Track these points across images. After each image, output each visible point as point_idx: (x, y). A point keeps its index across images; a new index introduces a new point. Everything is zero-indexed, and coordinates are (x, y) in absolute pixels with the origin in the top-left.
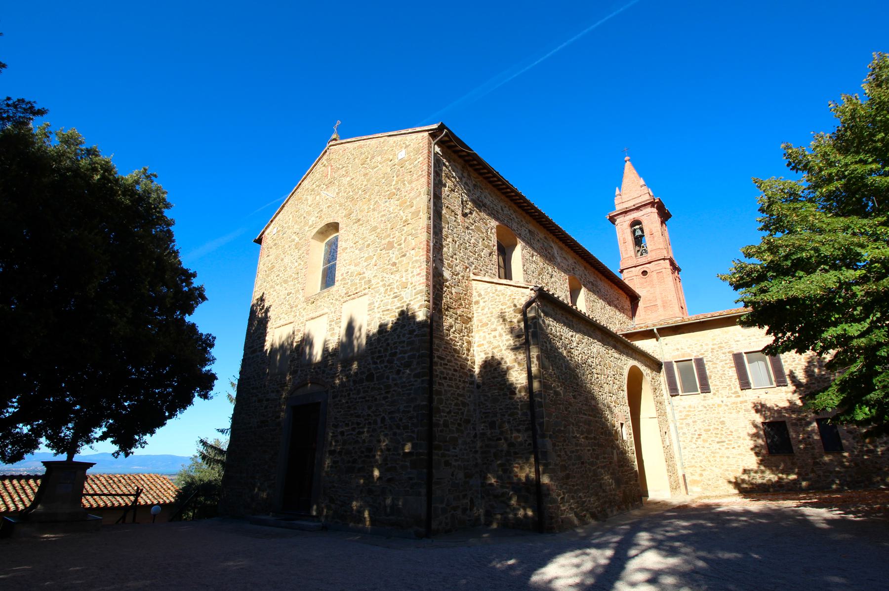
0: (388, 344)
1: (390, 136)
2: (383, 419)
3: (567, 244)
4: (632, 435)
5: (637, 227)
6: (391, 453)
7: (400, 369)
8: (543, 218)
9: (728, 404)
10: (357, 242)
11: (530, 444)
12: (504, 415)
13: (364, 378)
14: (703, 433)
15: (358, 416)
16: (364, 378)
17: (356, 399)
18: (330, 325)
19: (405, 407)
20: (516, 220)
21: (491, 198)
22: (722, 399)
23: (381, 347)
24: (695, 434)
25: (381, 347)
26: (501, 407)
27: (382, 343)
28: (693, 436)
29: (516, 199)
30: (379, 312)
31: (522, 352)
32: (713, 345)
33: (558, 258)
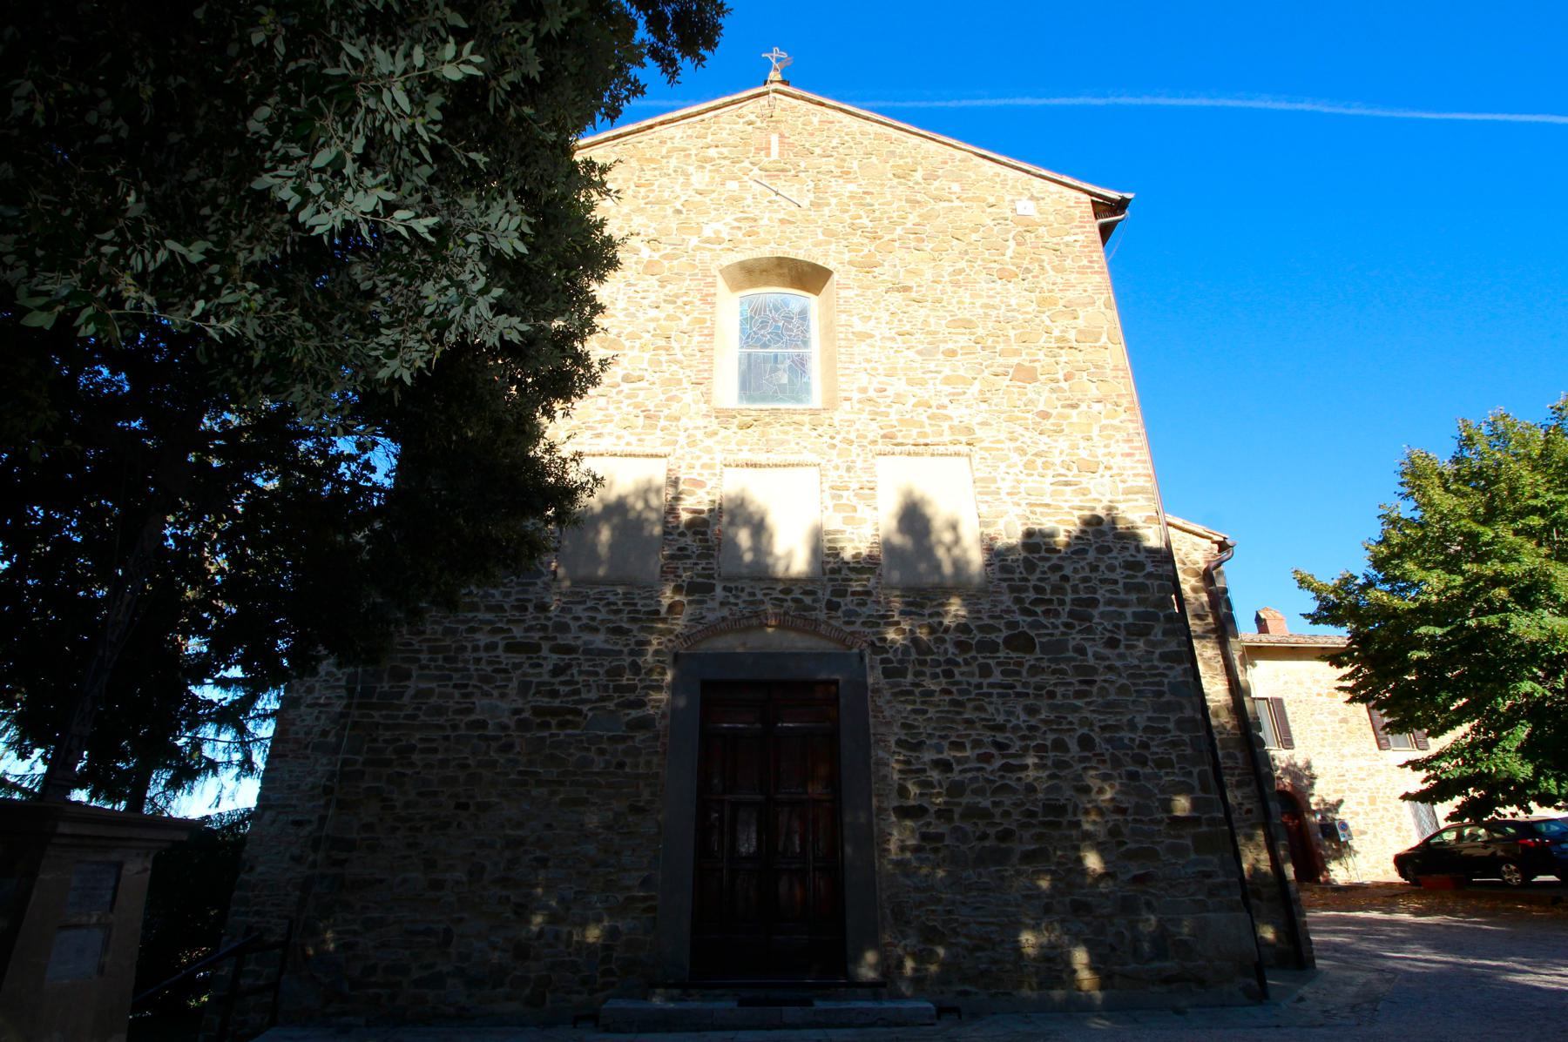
1: (984, 157)
6: (1130, 818)
13: (1000, 641)
16: (1000, 641)
19: (1150, 719)
31: (1209, 645)
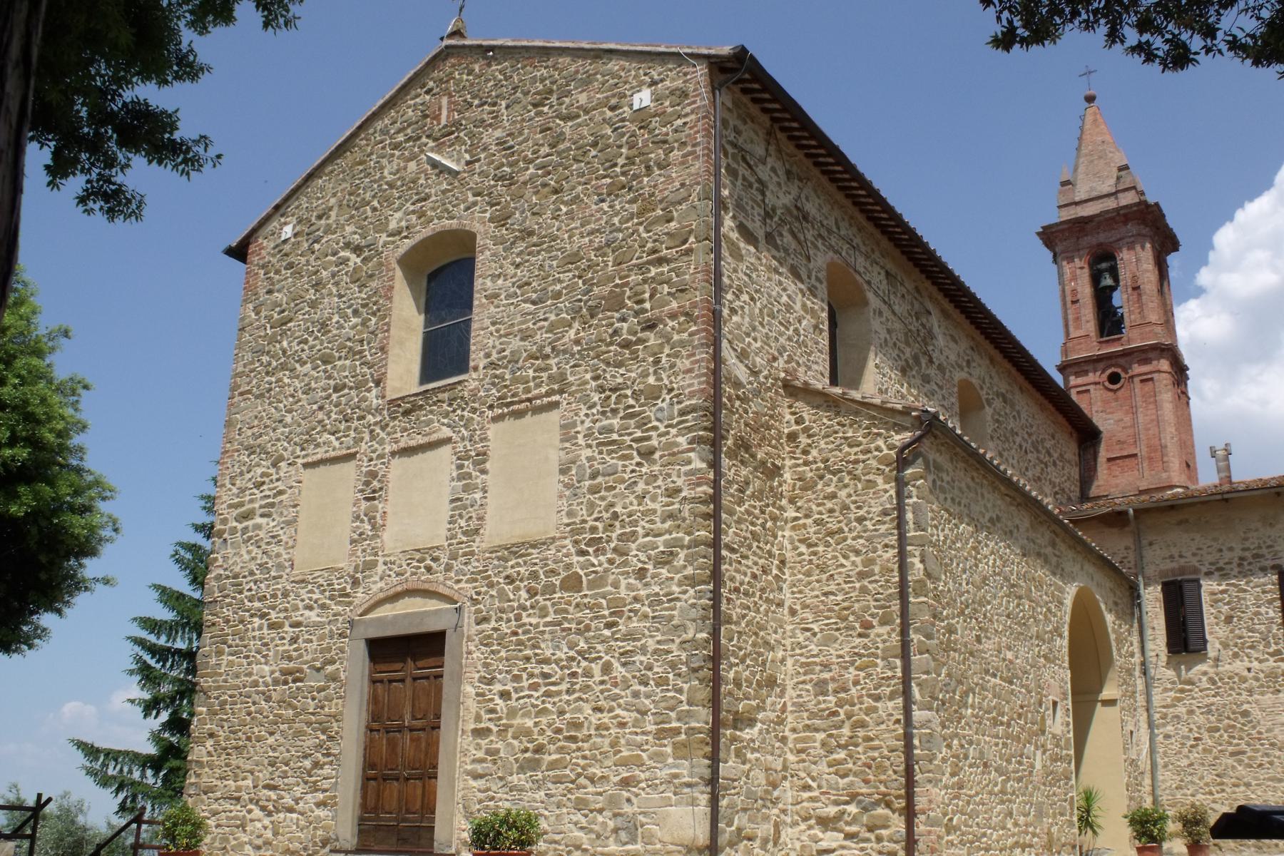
0: (615, 516)
2: (607, 669)
3: (958, 305)
4: (1071, 726)
5: (1104, 265)
7: (646, 566)
8: (917, 247)
9: (1262, 675)
10: (528, 284)
11: (898, 721)
12: (847, 668)
13: (558, 583)
14: (1206, 735)
15: (546, 661)
17: (537, 626)
18: (460, 467)
20: (863, 249)
21: (817, 201)
22: (1249, 665)
23: (596, 520)
24: (1188, 738)
25: (596, 520)
26: (841, 652)
27: (600, 512)
28: (1185, 741)
29: (927, 266)
30: (589, 446)
32: (1244, 550)
33: (940, 337)
